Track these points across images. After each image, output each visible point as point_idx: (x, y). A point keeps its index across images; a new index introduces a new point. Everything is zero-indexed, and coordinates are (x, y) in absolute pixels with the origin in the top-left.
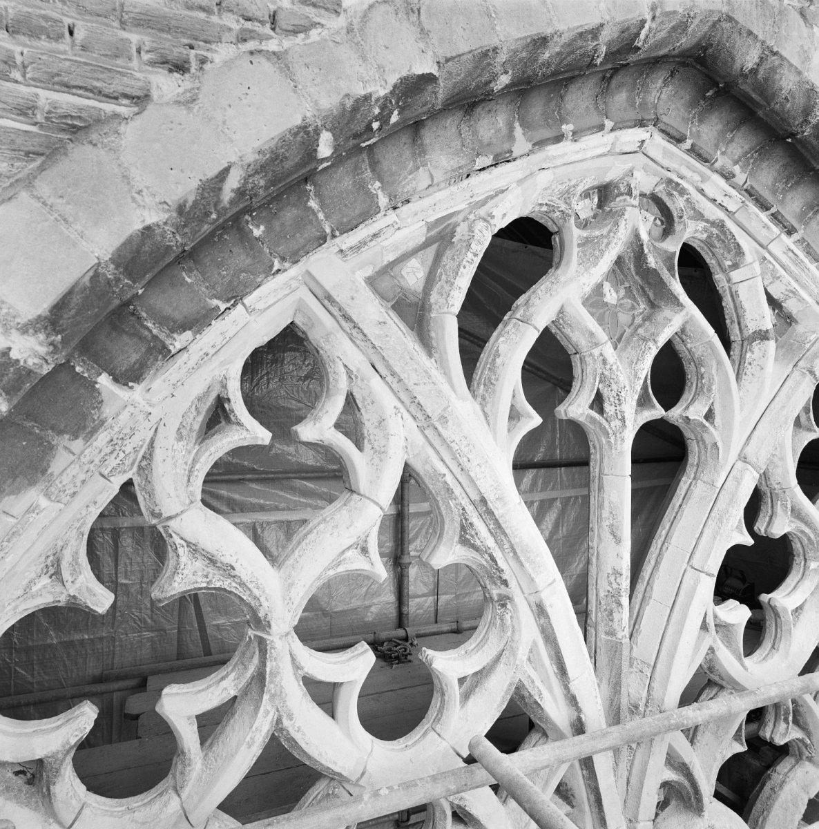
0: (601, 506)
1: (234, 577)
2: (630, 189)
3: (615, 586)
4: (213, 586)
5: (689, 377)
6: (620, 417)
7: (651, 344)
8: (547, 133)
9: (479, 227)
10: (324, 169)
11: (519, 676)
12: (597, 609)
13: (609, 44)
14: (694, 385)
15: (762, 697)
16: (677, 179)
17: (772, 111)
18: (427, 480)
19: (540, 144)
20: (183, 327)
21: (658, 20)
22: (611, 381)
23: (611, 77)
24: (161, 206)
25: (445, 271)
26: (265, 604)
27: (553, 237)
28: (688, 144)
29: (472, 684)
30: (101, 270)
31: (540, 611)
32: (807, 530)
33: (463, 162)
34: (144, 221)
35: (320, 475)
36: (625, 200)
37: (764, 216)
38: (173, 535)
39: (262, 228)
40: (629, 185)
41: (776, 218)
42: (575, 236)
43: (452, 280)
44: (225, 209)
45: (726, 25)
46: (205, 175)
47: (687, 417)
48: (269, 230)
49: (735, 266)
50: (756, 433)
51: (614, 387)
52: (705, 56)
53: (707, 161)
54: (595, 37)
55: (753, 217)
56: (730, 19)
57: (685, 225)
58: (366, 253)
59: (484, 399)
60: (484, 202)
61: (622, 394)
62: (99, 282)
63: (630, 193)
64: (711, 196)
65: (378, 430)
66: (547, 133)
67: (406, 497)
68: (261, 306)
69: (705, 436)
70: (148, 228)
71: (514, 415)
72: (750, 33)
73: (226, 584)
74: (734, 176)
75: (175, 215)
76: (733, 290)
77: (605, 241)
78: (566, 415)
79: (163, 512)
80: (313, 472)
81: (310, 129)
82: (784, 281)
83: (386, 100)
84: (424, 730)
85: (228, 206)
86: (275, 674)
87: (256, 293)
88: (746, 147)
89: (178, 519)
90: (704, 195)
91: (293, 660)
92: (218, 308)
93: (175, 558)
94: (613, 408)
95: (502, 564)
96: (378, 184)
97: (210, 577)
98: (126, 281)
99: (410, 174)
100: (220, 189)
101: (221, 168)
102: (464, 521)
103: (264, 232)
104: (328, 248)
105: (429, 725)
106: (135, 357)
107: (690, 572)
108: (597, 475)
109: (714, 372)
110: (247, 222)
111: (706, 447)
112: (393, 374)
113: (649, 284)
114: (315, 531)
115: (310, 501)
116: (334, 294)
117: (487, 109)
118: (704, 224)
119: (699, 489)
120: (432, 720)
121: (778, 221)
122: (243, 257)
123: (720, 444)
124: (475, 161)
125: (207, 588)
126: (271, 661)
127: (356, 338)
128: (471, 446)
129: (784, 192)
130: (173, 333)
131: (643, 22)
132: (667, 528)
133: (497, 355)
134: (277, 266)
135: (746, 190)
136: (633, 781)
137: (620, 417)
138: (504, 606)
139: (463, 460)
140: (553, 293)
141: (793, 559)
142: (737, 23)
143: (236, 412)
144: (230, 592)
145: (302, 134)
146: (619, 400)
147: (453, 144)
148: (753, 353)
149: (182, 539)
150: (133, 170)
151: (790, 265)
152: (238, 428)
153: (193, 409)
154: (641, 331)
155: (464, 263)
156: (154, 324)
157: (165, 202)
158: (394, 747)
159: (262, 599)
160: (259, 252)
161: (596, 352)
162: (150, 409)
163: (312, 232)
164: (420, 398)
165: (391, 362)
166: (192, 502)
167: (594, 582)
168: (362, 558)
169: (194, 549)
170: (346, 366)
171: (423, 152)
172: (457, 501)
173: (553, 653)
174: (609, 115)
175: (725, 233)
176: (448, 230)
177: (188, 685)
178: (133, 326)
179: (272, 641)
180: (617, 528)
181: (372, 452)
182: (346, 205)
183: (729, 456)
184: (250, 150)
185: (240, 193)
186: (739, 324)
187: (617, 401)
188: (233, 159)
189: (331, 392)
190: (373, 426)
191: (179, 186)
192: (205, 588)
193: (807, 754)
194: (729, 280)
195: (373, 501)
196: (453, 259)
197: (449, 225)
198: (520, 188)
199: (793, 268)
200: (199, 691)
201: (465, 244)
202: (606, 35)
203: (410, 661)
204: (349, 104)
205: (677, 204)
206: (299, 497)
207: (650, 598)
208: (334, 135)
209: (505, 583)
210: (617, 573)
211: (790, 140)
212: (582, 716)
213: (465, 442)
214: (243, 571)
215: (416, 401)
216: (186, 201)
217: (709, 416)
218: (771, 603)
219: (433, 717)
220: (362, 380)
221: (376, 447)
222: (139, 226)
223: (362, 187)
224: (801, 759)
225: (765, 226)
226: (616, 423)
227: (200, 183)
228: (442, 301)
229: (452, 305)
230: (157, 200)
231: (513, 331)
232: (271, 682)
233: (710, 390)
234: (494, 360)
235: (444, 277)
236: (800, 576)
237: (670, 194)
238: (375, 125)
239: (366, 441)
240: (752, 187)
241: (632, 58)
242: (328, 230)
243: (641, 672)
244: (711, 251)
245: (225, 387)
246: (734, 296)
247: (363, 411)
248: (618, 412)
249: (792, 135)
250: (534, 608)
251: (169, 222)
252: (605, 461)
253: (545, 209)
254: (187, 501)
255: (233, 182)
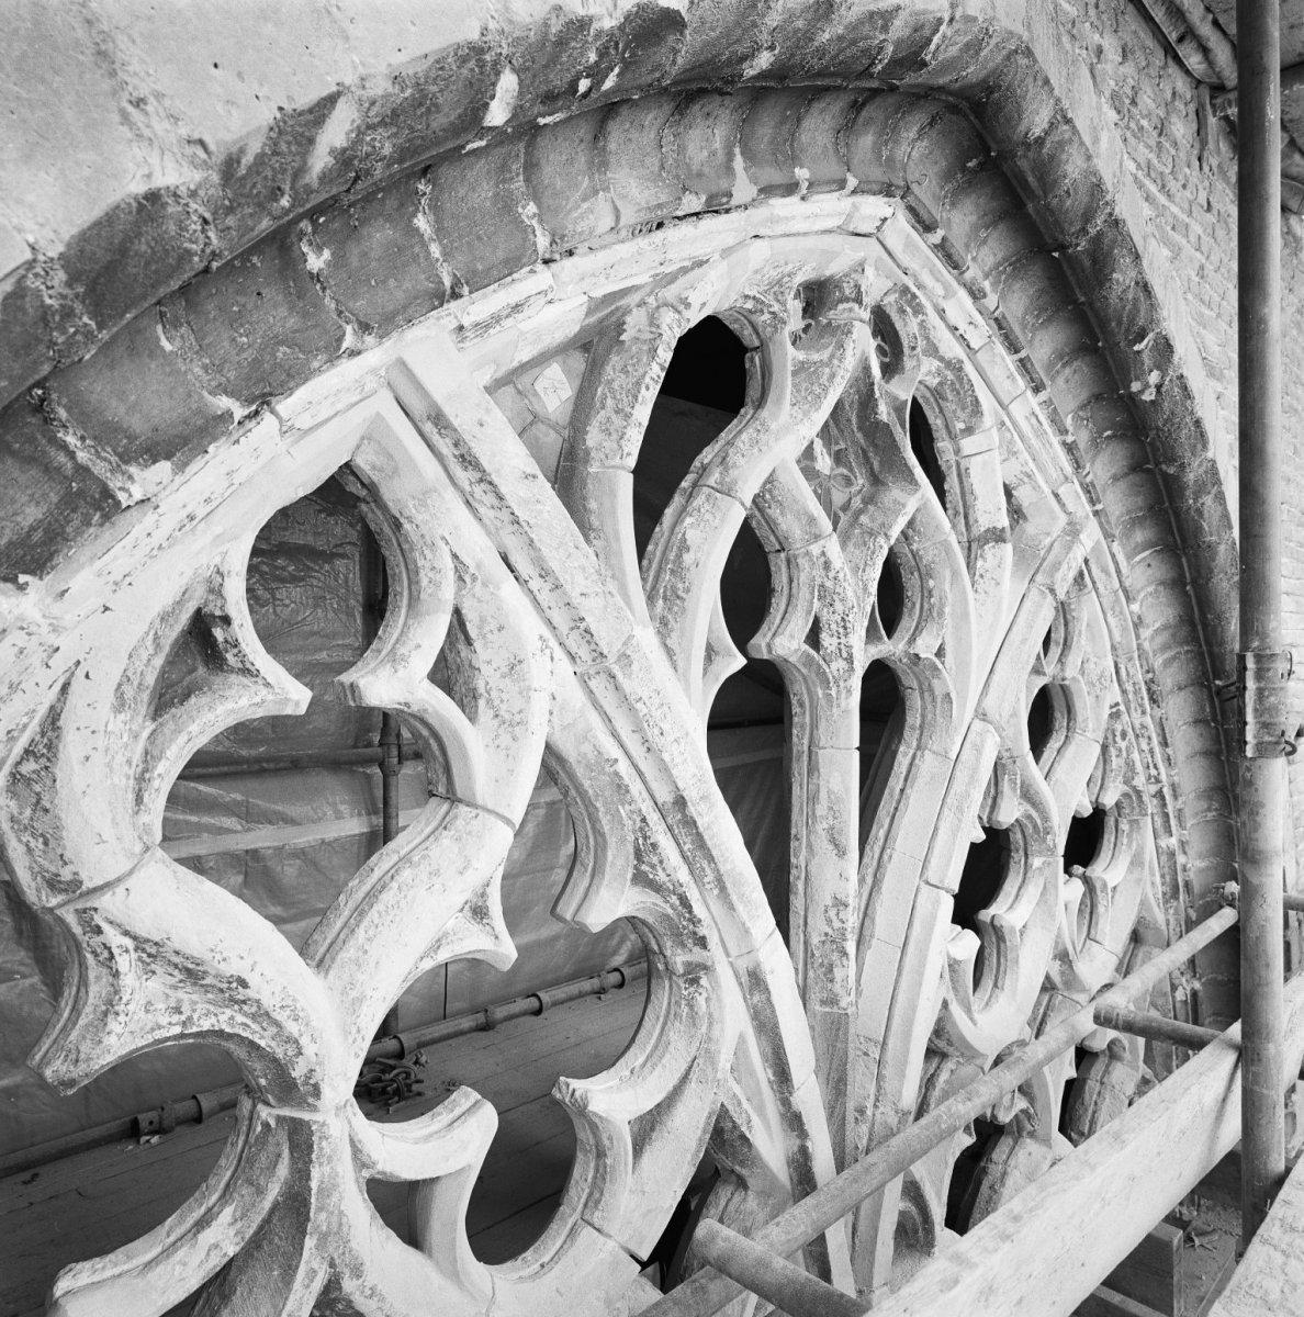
0: (813, 799)
1: (244, 1002)
2: (859, 293)
3: (837, 924)
4: (195, 1029)
5: (909, 594)
6: (845, 655)
7: (881, 540)
8: (774, 176)
9: (668, 321)
10: (474, 151)
11: (722, 1098)
12: (806, 964)
13: (898, 43)
14: (918, 606)
15: (1031, 1064)
16: (914, 289)
17: (1047, 206)
18: (580, 772)
19: (767, 191)
20: (154, 451)
21: (956, 25)
22: (835, 597)
23: (864, 104)
24: (189, 150)
25: (612, 390)
26: (309, 1049)
27: (748, 355)
28: (936, 238)
29: (646, 1128)
30: (31, 283)
31: (755, 981)
32: (1035, 814)
33: (663, 198)
34: (149, 176)
35: (232, 769)
36: (851, 310)
37: (1010, 361)
38: (105, 926)
39: (327, 254)
40: (858, 287)
41: (1024, 366)
42: (790, 357)
43: (628, 409)
44: (309, 190)
45: (1022, 61)
46: (290, 98)
47: (917, 655)
48: (338, 261)
49: (969, 431)
50: (996, 678)
51: (838, 606)
52: (986, 103)
53: (956, 267)
54: (885, 28)
55: (998, 360)
56: (1029, 53)
57: (918, 360)
58: (496, 339)
59: (666, 625)
60: (671, 279)
61: (850, 618)
62: (22, 309)
63: (858, 300)
64: (953, 321)
65: (507, 680)
66: (774, 176)
67: (393, 802)
68: (304, 422)
69: (935, 682)
70: (153, 197)
71: (711, 653)
72: (1047, 82)
73: (226, 1020)
74: (985, 296)
75: (215, 178)
76: (963, 467)
77: (827, 370)
78: (770, 651)
79: (83, 876)
80: (218, 764)
81: (488, 57)
82: (1021, 457)
83: (611, 39)
84: (569, 1226)
85: (315, 185)
86: (325, 1192)
87: (302, 394)
88: (1000, 256)
89: (120, 890)
90: (943, 319)
91: (356, 1151)
92: (229, 415)
93: (106, 979)
94: (835, 641)
95: (699, 910)
96: (532, 208)
97: (186, 1008)
98: (85, 319)
99: (584, 200)
100: (311, 141)
101: (324, 94)
102: (641, 841)
103: (328, 264)
104: (438, 319)
105: (576, 1216)
106: (32, 514)
107: (925, 889)
108: (806, 748)
109: (947, 587)
110: (302, 234)
111: (934, 700)
112: (545, 574)
113: (876, 446)
114: (394, 885)
115: (206, 819)
116: (448, 411)
117: (706, 110)
118: (936, 363)
119: (927, 763)
120: (581, 1206)
121: (1026, 370)
122: (283, 311)
123: (953, 695)
124: (680, 199)
125: (182, 1036)
126: (321, 1165)
127: (481, 502)
128: (665, 708)
129: (1034, 330)
130: (127, 462)
131: (940, 21)
132: (886, 826)
133: (684, 547)
134: (349, 341)
135: (996, 320)
136: (862, 1228)
137: (845, 655)
138: (695, 981)
139: (652, 733)
140: (764, 449)
141: (1009, 856)
142: (1035, 61)
143: (243, 645)
144: (230, 1036)
145: (472, 64)
146: (845, 628)
147: (648, 161)
148: (985, 560)
149: (126, 933)
150: (122, 40)
151: (1031, 436)
152: (245, 681)
153: (149, 641)
154: (864, 519)
155: (647, 380)
156: (83, 439)
157: (201, 143)
158: (522, 1273)
159: (304, 1041)
160: (315, 306)
161: (815, 549)
162: (54, 640)
163: (416, 280)
164: (591, 622)
165: (545, 551)
166: (147, 849)
167: (801, 922)
168: (475, 927)
169: (151, 951)
170: (455, 556)
171: (604, 165)
172: (633, 807)
173: (769, 1050)
174: (852, 167)
175: (960, 379)
176: (614, 319)
177: (111, 1256)
178: (32, 440)
179: (324, 1124)
180: (840, 832)
181: (496, 722)
182: (479, 238)
183: (964, 712)
184: (383, 69)
185: (344, 159)
186: (966, 517)
187: (841, 630)
188: (349, 79)
189: (423, 608)
190: (498, 674)
191: (234, 112)
192: (175, 1037)
193: (1029, 1127)
194: (957, 451)
195: (498, 815)
196: (624, 371)
197: (617, 309)
198: (725, 263)
199: (1034, 441)
200: (148, 1265)
201: (645, 348)
202: (899, 28)
203: (419, 1094)
204: (556, 27)
205: (907, 328)
206: (184, 812)
207: (872, 936)
208: (521, 82)
209: (702, 942)
210: (840, 904)
211: (1056, 255)
212: (809, 1144)
213: (657, 701)
214: (264, 991)
215: (583, 626)
216: (242, 151)
217: (940, 653)
218: (996, 923)
219: (583, 1200)
220: (485, 585)
221: (502, 713)
222: (138, 188)
223: (507, 206)
224: (1020, 1136)
225: (1010, 376)
226: (838, 665)
227: (278, 116)
228: (609, 445)
229: (629, 454)
230: (184, 131)
231: (707, 506)
232: (320, 1209)
233: (941, 614)
234: (679, 556)
235: (610, 402)
236: (1020, 880)
237: (902, 311)
238: (584, 85)
239: (482, 703)
240: (1004, 317)
241: (911, 79)
242: (447, 282)
243: (866, 1054)
244: (939, 405)
245: (216, 591)
246: (962, 476)
247: (477, 645)
248: (842, 647)
249: (1062, 248)
250: (745, 979)
251: (201, 193)
252: (822, 725)
253: (749, 305)
254: (138, 848)
255: (335, 133)
